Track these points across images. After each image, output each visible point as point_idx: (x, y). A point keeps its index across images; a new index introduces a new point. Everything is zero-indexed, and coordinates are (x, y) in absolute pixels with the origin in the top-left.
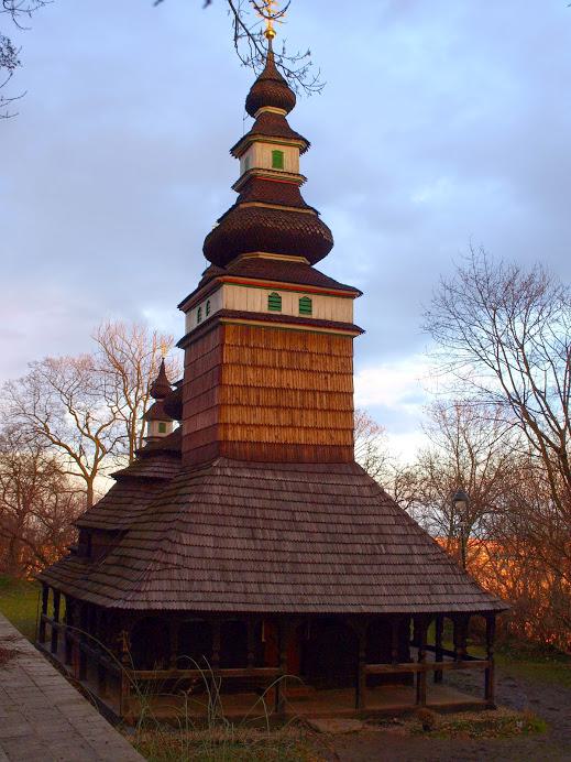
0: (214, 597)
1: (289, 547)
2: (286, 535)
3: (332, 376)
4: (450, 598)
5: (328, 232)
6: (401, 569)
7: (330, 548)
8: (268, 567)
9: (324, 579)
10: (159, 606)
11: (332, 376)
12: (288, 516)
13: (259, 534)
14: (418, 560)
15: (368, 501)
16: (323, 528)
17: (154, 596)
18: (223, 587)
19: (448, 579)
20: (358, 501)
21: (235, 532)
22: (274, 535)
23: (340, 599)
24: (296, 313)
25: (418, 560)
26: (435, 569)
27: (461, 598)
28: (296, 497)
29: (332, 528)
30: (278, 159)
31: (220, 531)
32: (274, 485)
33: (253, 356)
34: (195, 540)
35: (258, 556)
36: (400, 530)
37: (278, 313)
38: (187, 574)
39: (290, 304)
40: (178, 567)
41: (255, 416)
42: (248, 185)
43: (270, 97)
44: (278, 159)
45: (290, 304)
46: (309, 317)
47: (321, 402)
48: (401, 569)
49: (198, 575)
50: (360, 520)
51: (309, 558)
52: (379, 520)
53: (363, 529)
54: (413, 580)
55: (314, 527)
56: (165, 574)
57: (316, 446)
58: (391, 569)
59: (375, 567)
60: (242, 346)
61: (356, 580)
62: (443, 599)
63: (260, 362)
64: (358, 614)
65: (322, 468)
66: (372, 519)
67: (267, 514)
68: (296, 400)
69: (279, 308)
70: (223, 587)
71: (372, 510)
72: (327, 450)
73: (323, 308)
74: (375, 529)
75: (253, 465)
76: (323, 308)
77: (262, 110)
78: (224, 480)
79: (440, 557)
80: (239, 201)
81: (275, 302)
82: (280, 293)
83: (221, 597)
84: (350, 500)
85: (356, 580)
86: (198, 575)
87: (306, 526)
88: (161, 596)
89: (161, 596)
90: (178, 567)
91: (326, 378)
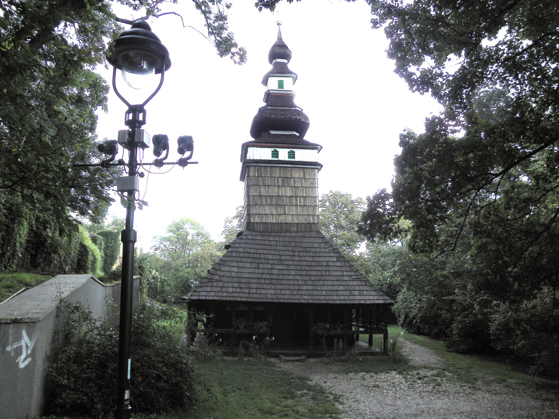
0: (232, 294)
1: (276, 272)
2: (275, 267)
3: (306, 189)
4: (360, 297)
5: (306, 118)
6: (336, 283)
7: (298, 273)
8: (263, 281)
9: (292, 288)
10: (204, 298)
11: (306, 189)
12: (278, 257)
13: (261, 266)
14: (346, 278)
15: (322, 250)
16: (296, 263)
17: (202, 294)
18: (238, 290)
19: (361, 288)
20: (317, 250)
21: (248, 265)
22: (269, 266)
23: (299, 297)
24: (287, 159)
25: (346, 278)
26: (356, 283)
27: (367, 297)
28: (284, 248)
29: (300, 263)
30: (281, 84)
31: (241, 265)
32: (273, 243)
33: (263, 181)
34: (227, 269)
35: (259, 276)
36: (339, 264)
37: (277, 159)
38: (220, 284)
39: (283, 154)
40: (217, 281)
41: (265, 210)
42: (269, 97)
43: (294, 84)
44: (281, 84)
45: (283, 154)
46: (293, 160)
47: (300, 202)
48: (336, 283)
49: (226, 285)
50: (317, 259)
51: (286, 277)
52: (327, 259)
53: (317, 264)
54: (341, 288)
55: (291, 263)
56: (210, 284)
57: (298, 224)
58: (330, 283)
59: (321, 282)
60: (258, 176)
61: (310, 288)
62: (357, 298)
63: (267, 183)
64: (272, 303)
65: (268, 234)
66: (324, 259)
67: (267, 256)
68: (287, 201)
69: (294, 158)
70: (238, 290)
71: (324, 254)
72: (269, 226)
73: (301, 155)
74: (325, 264)
75: (263, 234)
76: (301, 155)
77: (274, 61)
78: (247, 241)
79: (359, 277)
80: (266, 106)
81: (275, 154)
82: (278, 149)
83: (235, 295)
84: (312, 250)
85: (310, 288)
86: (226, 285)
87: (287, 263)
88: (205, 294)
89: (205, 294)
90: (217, 281)
91: (303, 190)
